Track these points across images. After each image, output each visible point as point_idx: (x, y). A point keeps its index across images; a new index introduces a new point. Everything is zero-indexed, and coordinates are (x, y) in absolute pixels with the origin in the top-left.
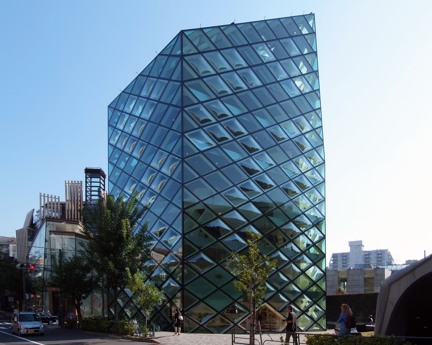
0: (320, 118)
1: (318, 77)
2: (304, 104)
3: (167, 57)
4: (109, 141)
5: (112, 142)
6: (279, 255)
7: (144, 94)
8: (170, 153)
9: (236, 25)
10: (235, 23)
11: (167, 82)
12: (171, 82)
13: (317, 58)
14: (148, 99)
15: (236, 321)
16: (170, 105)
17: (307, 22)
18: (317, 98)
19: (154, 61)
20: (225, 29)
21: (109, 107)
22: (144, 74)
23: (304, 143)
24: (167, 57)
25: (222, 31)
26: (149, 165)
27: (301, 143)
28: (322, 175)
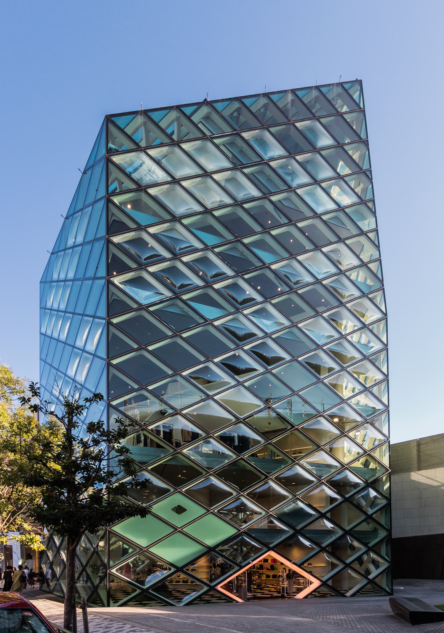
20: (350, 88)
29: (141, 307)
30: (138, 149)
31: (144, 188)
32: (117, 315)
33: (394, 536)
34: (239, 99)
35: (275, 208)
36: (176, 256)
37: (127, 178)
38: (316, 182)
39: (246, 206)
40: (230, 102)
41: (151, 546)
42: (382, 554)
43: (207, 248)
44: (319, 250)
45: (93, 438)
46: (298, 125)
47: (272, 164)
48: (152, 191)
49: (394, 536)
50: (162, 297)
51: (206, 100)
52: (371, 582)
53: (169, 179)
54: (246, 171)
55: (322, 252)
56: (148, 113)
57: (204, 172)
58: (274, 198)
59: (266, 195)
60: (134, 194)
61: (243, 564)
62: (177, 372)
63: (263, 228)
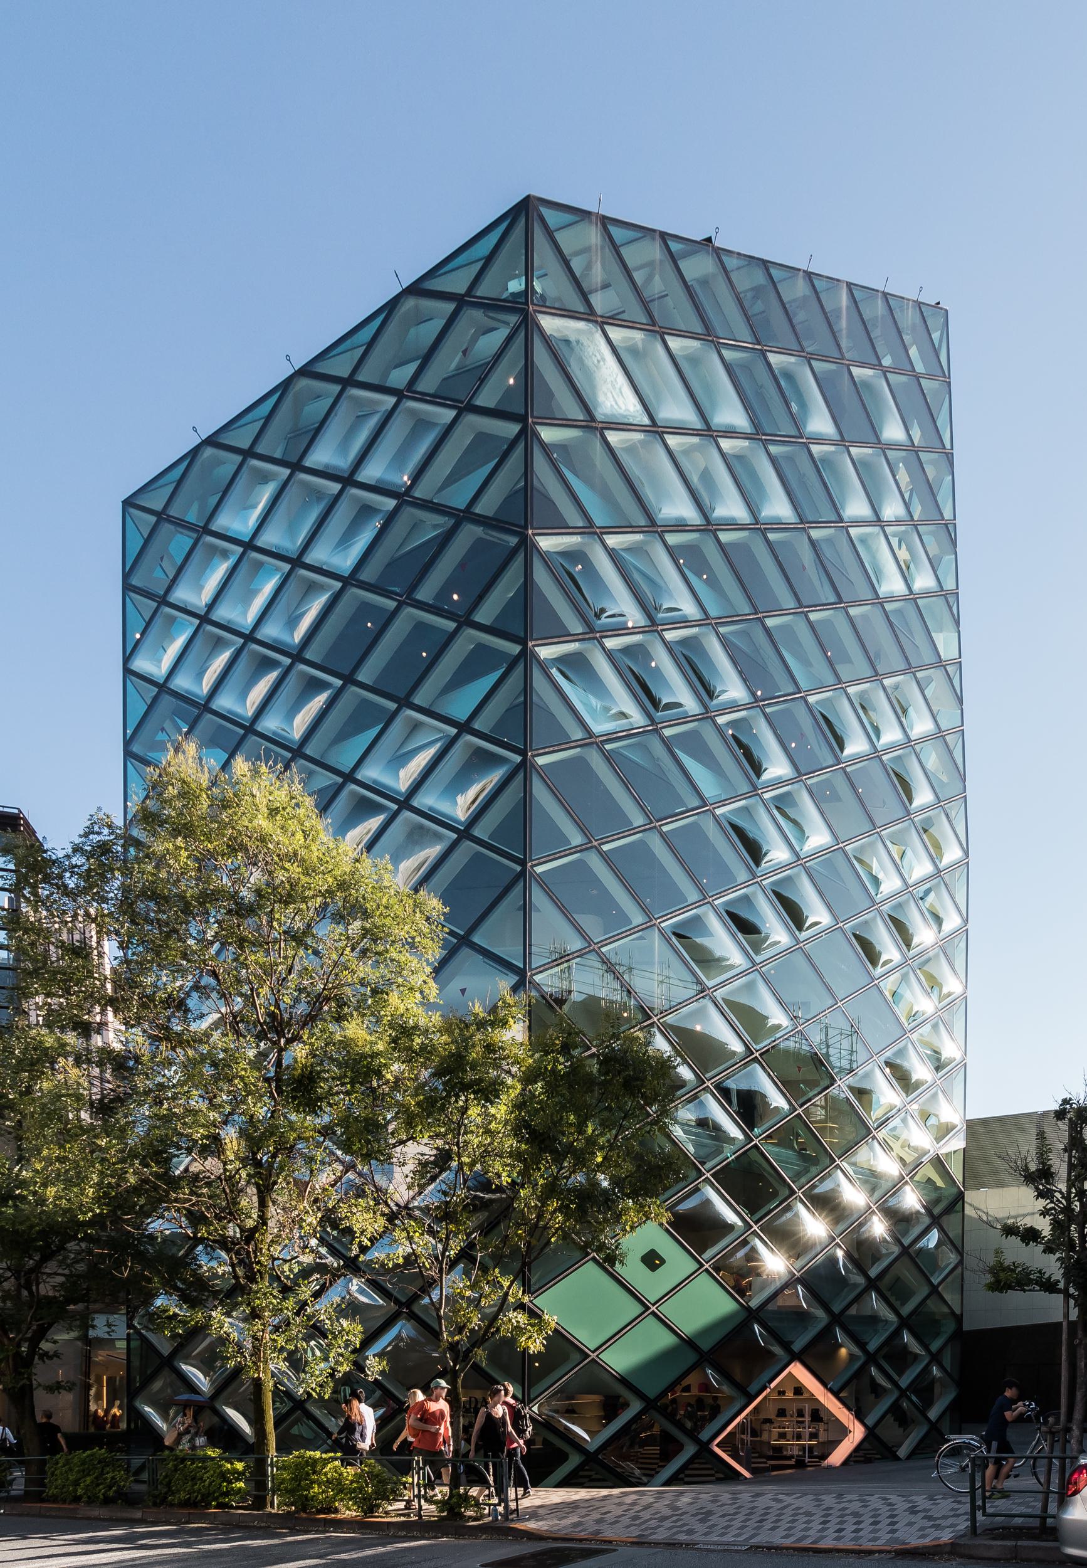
0: (957, 695)
1: (954, 543)
2: (911, 633)
3: (449, 307)
4: (127, 659)
5: (141, 664)
6: (708, 1202)
7: (322, 455)
8: (464, 727)
9: (719, 252)
10: (718, 243)
11: (336, 487)
12: (471, 419)
13: (950, 477)
14: (348, 480)
15: (704, 1436)
16: (465, 516)
17: (926, 334)
18: (950, 623)
19: (442, 271)
20: (686, 255)
21: (128, 503)
22: (229, 439)
23: (759, 829)
24: (449, 307)
25: (673, 258)
26: (349, 777)
27: (752, 833)
28: (957, 899)
29: (591, 739)
30: (589, 315)
31: (601, 425)
32: (547, 750)
33: (966, 1327)
34: (765, 264)
35: (817, 560)
36: (653, 625)
37: (565, 382)
38: (878, 521)
39: (771, 536)
40: (577, 219)
41: (604, 1347)
42: (944, 1363)
43: (706, 620)
44: (656, 634)
45: (185, 1020)
46: (856, 371)
47: (815, 449)
48: (613, 437)
49: (966, 1327)
50: (623, 723)
51: (709, 240)
52: (168, 1363)
53: (646, 421)
54: (773, 449)
55: (663, 640)
56: (541, 209)
57: (706, 428)
58: (815, 534)
59: (803, 523)
60: (581, 434)
61: (752, 1389)
62: (654, 922)
63: (799, 603)
